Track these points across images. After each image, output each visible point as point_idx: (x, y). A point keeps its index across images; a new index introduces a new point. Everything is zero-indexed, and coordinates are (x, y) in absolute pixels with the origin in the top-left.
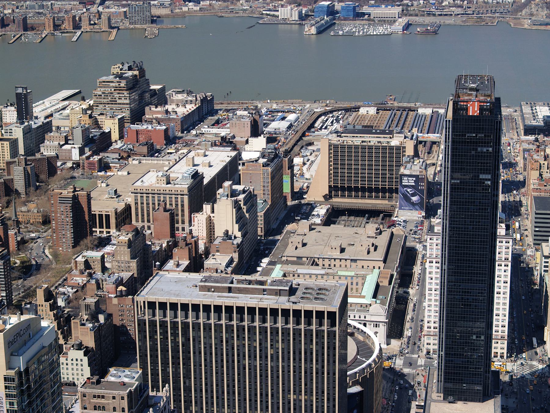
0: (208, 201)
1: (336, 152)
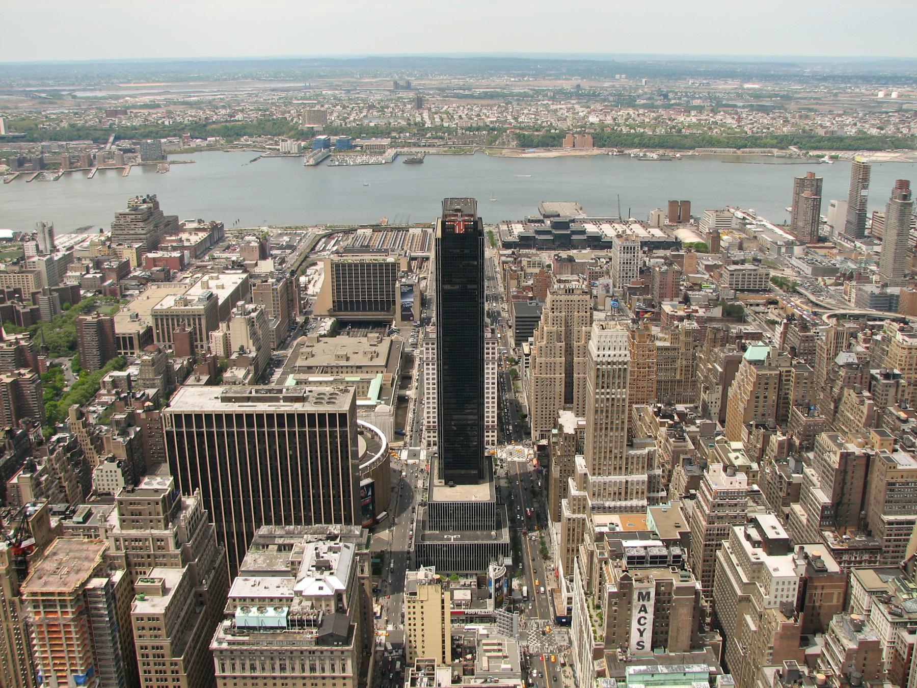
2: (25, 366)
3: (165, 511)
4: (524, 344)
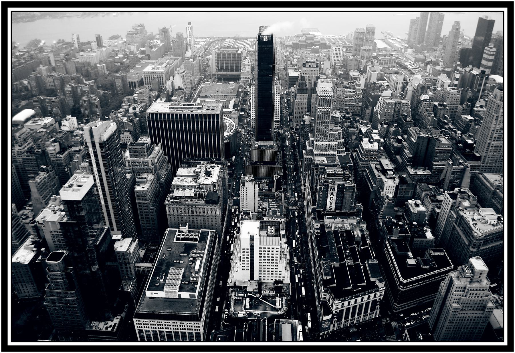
2: (93, 94)
3: (147, 151)
4: (292, 88)
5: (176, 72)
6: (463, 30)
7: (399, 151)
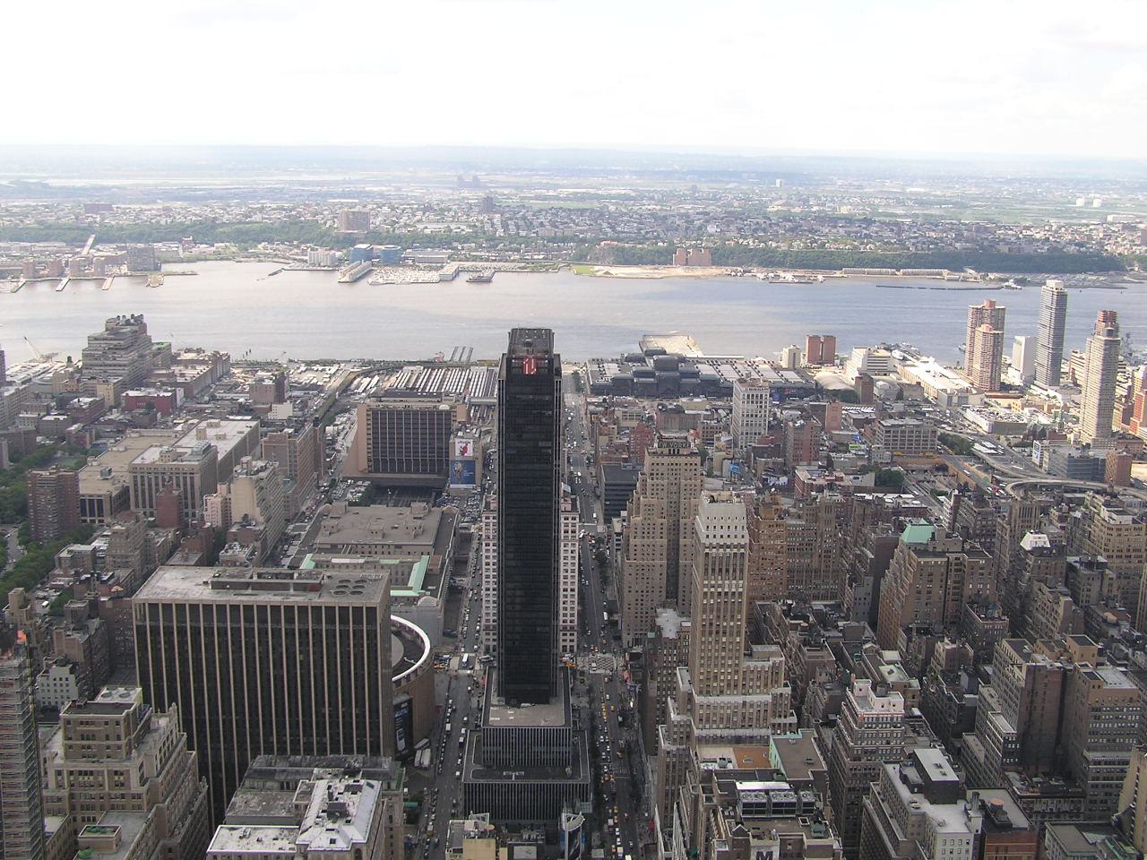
0: (222, 481)
1: (375, 419)
3: (128, 734)
5: (238, 468)
6: (1128, 336)
7: (970, 719)
